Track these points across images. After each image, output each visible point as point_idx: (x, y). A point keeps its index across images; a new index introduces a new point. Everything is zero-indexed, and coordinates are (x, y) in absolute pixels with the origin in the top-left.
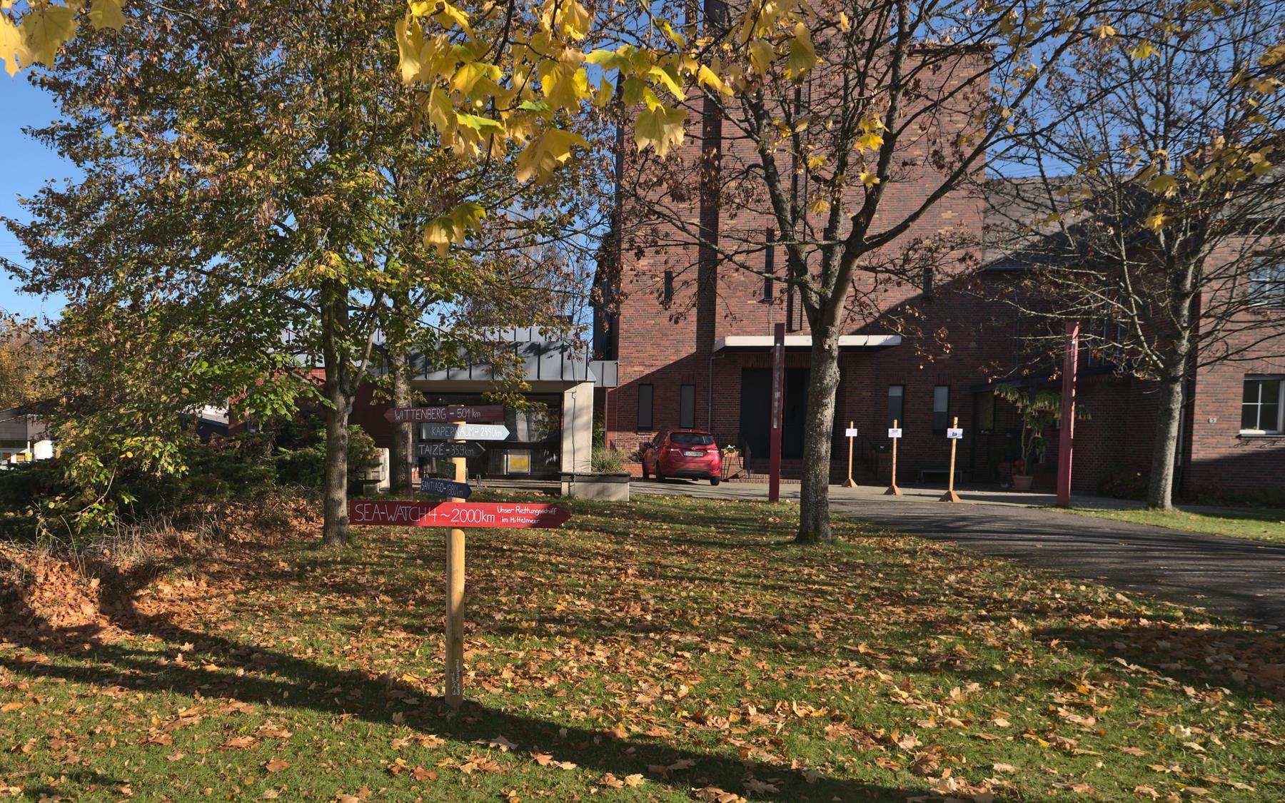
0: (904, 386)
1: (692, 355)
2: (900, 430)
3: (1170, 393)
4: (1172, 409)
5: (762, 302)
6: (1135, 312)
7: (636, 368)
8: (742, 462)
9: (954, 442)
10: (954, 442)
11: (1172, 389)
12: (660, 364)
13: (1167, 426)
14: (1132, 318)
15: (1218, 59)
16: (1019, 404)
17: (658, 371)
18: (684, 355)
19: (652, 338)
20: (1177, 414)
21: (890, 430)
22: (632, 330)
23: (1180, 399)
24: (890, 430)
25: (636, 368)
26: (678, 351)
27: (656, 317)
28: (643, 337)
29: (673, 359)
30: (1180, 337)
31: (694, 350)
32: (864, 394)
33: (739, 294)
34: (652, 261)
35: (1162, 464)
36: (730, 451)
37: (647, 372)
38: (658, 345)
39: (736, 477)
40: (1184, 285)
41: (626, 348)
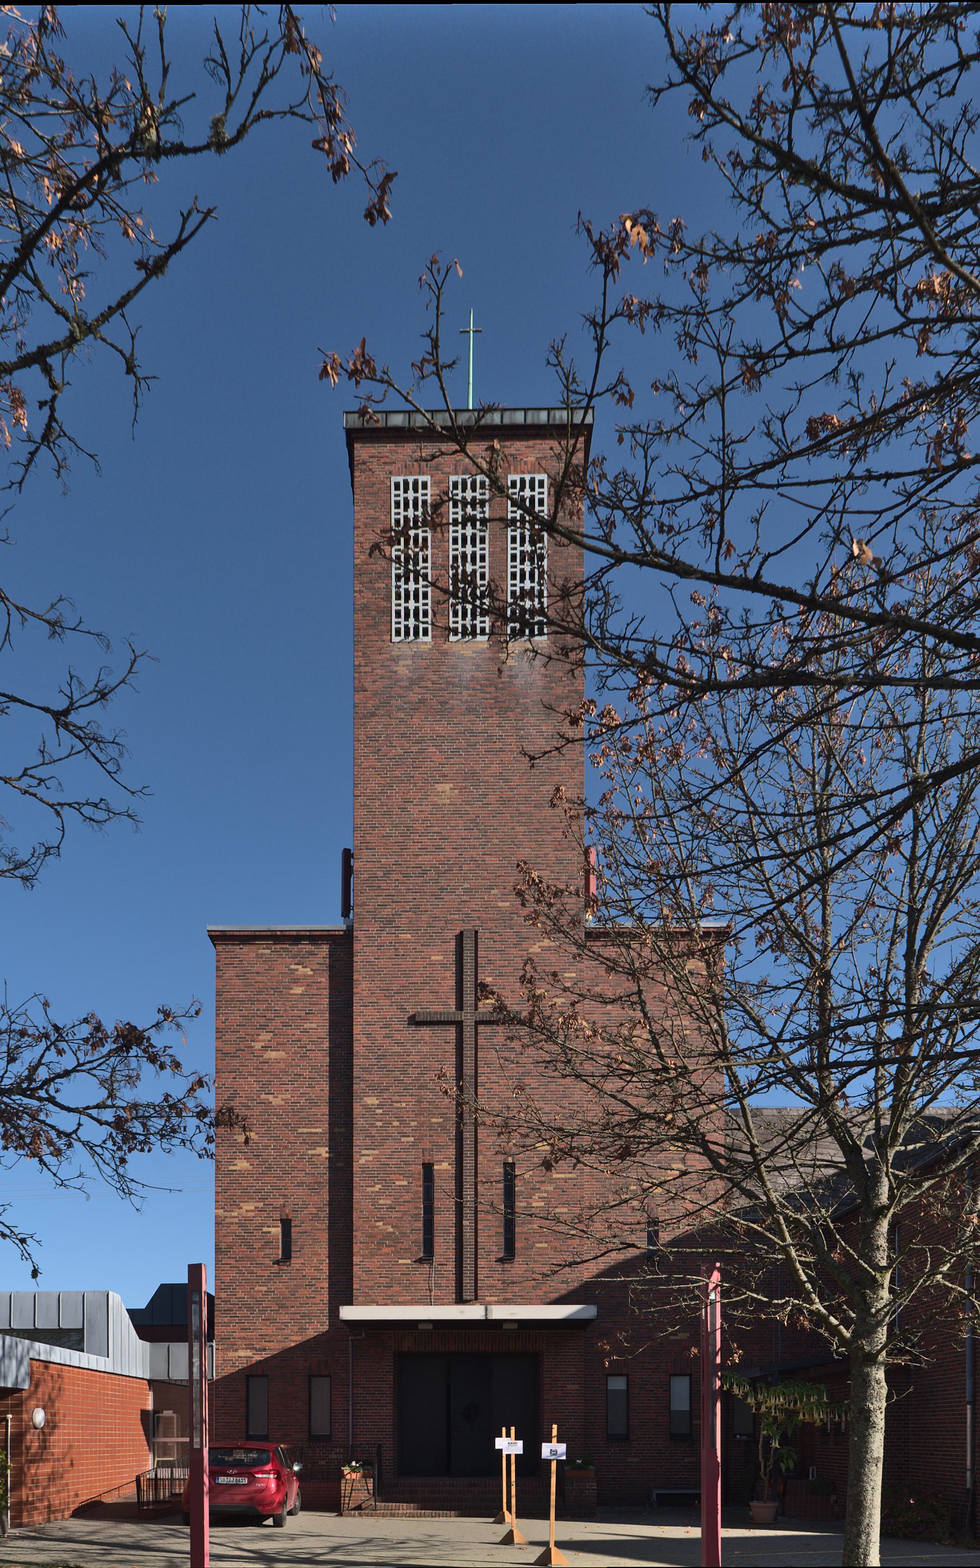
0: (627, 1376)
1: (323, 1334)
2: (520, 1443)
3: (865, 1382)
4: (869, 1411)
5: (420, 1261)
6: (789, 1240)
7: (242, 1353)
8: (371, 1486)
9: (554, 1466)
10: (554, 1466)
11: (868, 1375)
12: (274, 1348)
13: (864, 1441)
14: (784, 1250)
15: (701, 475)
16: (750, 1400)
17: (274, 1357)
18: (311, 1333)
19: (263, 1311)
20: (879, 1419)
21: (497, 1440)
22: (233, 1300)
23: (884, 1391)
24: (497, 1440)
25: (242, 1353)
26: (302, 1330)
27: (269, 1280)
28: (251, 1309)
29: (294, 1340)
30: (875, 1285)
31: (326, 1328)
32: (569, 1387)
33: (385, 1250)
34: (261, 1205)
35: (859, 1506)
36: (354, 1470)
37: (258, 1358)
38: (274, 1321)
39: (359, 1508)
40: (877, 1196)
41: (227, 1325)
